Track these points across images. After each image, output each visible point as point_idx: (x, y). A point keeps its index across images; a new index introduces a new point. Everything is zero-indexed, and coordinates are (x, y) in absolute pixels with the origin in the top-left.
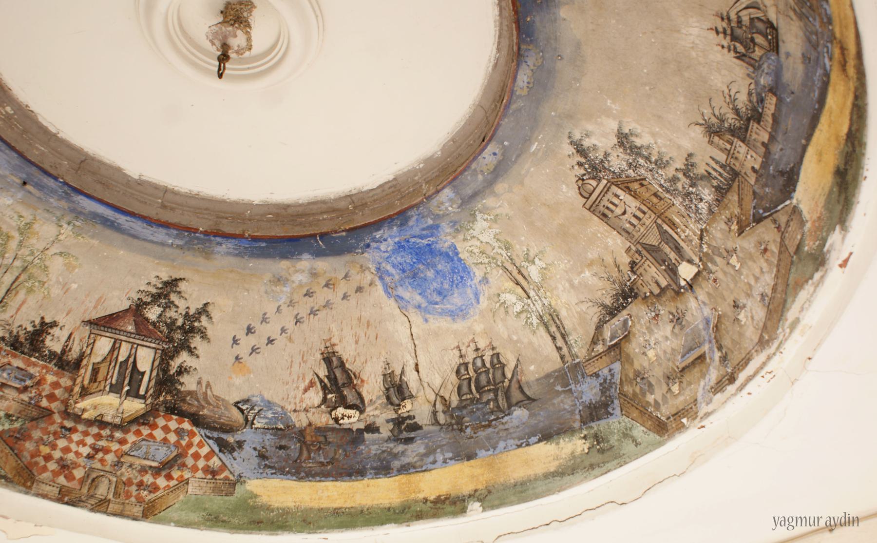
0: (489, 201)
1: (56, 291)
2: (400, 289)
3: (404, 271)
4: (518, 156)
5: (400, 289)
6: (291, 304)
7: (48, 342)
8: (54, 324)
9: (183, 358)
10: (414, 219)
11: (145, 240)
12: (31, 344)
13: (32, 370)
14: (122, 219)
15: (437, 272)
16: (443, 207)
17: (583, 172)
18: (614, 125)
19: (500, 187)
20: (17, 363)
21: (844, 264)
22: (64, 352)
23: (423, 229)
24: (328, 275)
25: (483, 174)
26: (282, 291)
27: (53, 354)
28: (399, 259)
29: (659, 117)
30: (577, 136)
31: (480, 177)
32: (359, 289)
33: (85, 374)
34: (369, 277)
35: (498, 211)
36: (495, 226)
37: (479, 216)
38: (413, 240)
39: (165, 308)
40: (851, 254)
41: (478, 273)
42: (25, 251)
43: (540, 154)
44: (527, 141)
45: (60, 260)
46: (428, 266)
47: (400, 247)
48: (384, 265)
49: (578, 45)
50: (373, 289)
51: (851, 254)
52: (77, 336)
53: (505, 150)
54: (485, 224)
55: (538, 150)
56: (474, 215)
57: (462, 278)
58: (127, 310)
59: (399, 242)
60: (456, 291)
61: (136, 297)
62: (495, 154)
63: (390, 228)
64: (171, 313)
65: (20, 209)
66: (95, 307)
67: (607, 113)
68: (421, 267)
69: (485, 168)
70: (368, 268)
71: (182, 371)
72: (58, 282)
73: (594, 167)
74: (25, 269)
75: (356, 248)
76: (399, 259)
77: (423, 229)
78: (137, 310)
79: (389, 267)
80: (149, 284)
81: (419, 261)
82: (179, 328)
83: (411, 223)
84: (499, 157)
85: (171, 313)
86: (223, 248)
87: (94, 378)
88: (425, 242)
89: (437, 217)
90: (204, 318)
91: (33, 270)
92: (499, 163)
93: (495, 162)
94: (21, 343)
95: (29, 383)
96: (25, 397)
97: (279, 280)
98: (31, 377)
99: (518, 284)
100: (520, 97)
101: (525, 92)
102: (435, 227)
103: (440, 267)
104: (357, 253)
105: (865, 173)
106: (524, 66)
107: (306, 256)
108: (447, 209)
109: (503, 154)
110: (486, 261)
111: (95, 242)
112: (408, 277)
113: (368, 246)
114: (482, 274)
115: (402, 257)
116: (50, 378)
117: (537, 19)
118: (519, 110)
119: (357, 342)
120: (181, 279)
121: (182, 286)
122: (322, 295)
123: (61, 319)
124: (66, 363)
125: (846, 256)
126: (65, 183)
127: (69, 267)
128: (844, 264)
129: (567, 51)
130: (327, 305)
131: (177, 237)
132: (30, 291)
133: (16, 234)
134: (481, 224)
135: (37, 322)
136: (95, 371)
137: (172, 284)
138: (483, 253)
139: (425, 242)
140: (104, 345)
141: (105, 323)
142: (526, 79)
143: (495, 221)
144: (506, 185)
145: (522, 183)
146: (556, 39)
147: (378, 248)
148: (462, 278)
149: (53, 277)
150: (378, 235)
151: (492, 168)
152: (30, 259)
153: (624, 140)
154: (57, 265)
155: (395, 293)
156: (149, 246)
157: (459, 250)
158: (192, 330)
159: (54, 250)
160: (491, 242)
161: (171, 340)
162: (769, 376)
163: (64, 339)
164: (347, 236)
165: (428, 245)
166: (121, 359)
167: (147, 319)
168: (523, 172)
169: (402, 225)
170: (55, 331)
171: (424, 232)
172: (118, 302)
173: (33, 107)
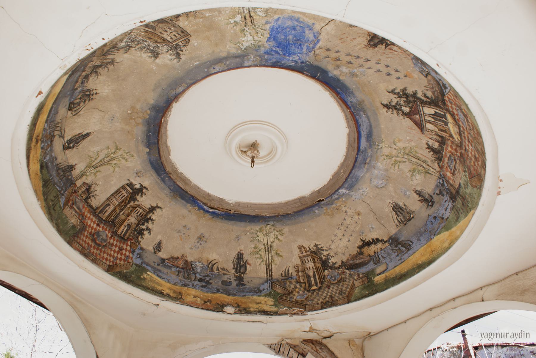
0: (234, 51)
1: (413, 144)
2: (310, 40)
3: (300, 45)
4: (205, 63)
5: (310, 40)
6: (361, 66)
7: (436, 147)
8: (427, 144)
9: (420, 95)
10: (271, 61)
11: (370, 122)
12: (438, 153)
13: (448, 155)
14: (364, 133)
15: (286, 36)
16: (255, 59)
17: (182, 48)
18: (158, 61)
19: (224, 54)
20: (446, 159)
21: (40, 93)
22: (438, 141)
23: (273, 55)
24: (333, 63)
25: (226, 63)
26: (358, 72)
27: (440, 146)
28: (296, 50)
29: (135, 62)
30: (176, 61)
31: (227, 63)
32: (328, 50)
33: (444, 134)
34: (318, 52)
35: (234, 46)
36: (240, 40)
37: (243, 48)
38: (282, 53)
39: (401, 106)
40: (37, 97)
41: (268, 27)
42: (400, 155)
43: (196, 60)
44: (197, 67)
45: (398, 144)
46: (288, 41)
47: (290, 54)
48: (305, 52)
49: (154, 90)
50: (322, 46)
51: (37, 97)
52: (430, 136)
53: (208, 68)
54: (244, 43)
55: (196, 62)
56: (246, 49)
57: (277, 29)
58: (410, 119)
59: (288, 56)
60: (285, 26)
61: (402, 117)
62: (214, 68)
63: (284, 64)
64: (402, 103)
65: (380, 160)
66: (414, 130)
67: (157, 65)
68: (291, 42)
69: (223, 65)
70: (314, 54)
71: (425, 96)
72: (409, 143)
73: (176, 48)
74: (407, 154)
75: (308, 65)
76: (296, 50)
77: (273, 55)
78: (408, 115)
79: (305, 50)
80: (392, 114)
81: (289, 44)
82: (407, 99)
83: (274, 60)
84: (213, 66)
85: (402, 103)
86: (354, 100)
87: (445, 131)
88: (278, 49)
89: (260, 56)
90: (396, 91)
91: (407, 152)
92: (215, 64)
93: (217, 65)
94: (439, 157)
95: (453, 158)
96: (458, 161)
97: (353, 75)
98: (450, 156)
99: (251, 17)
100: (187, 84)
101: (184, 84)
102: (267, 53)
103: (283, 37)
104: (310, 63)
105: (28, 127)
106: (177, 93)
107: (330, 75)
108: (254, 58)
109: (211, 66)
110: (258, 29)
111: (383, 136)
112: (301, 41)
113: (302, 62)
114: (266, 25)
115: (294, 50)
116: (449, 149)
117: (162, 103)
118: (191, 79)
119: (355, 39)
120: (382, 104)
121: (385, 102)
122: (345, 59)
123: (424, 142)
124: (442, 142)
125: (39, 96)
126: (357, 154)
127: (400, 141)
128: (40, 93)
129: (159, 90)
130: (348, 55)
131: (359, 115)
132: (416, 152)
133: (393, 159)
134: (246, 44)
135: (428, 150)
136: (442, 130)
137: (387, 106)
138: (258, 33)
139: (278, 49)
140: (429, 126)
141: (420, 126)
142: (180, 89)
143: (239, 43)
144: (221, 54)
145: (213, 52)
146: (160, 95)
147: (299, 59)
148: (277, 29)
149: (407, 145)
150: (293, 64)
151: (220, 64)
152: (402, 154)
153: (156, 55)
154: (400, 145)
155: (315, 40)
156: (372, 121)
157: (266, 39)
158: (405, 94)
159: (394, 146)
160: (249, 35)
161: (414, 102)
162: (89, 48)
163: (433, 141)
164: (305, 71)
165: (278, 47)
166: (433, 120)
167: (410, 111)
168: (209, 56)
169: (278, 62)
170: (430, 144)
171: (274, 53)
172: (408, 122)
173: (339, 164)
